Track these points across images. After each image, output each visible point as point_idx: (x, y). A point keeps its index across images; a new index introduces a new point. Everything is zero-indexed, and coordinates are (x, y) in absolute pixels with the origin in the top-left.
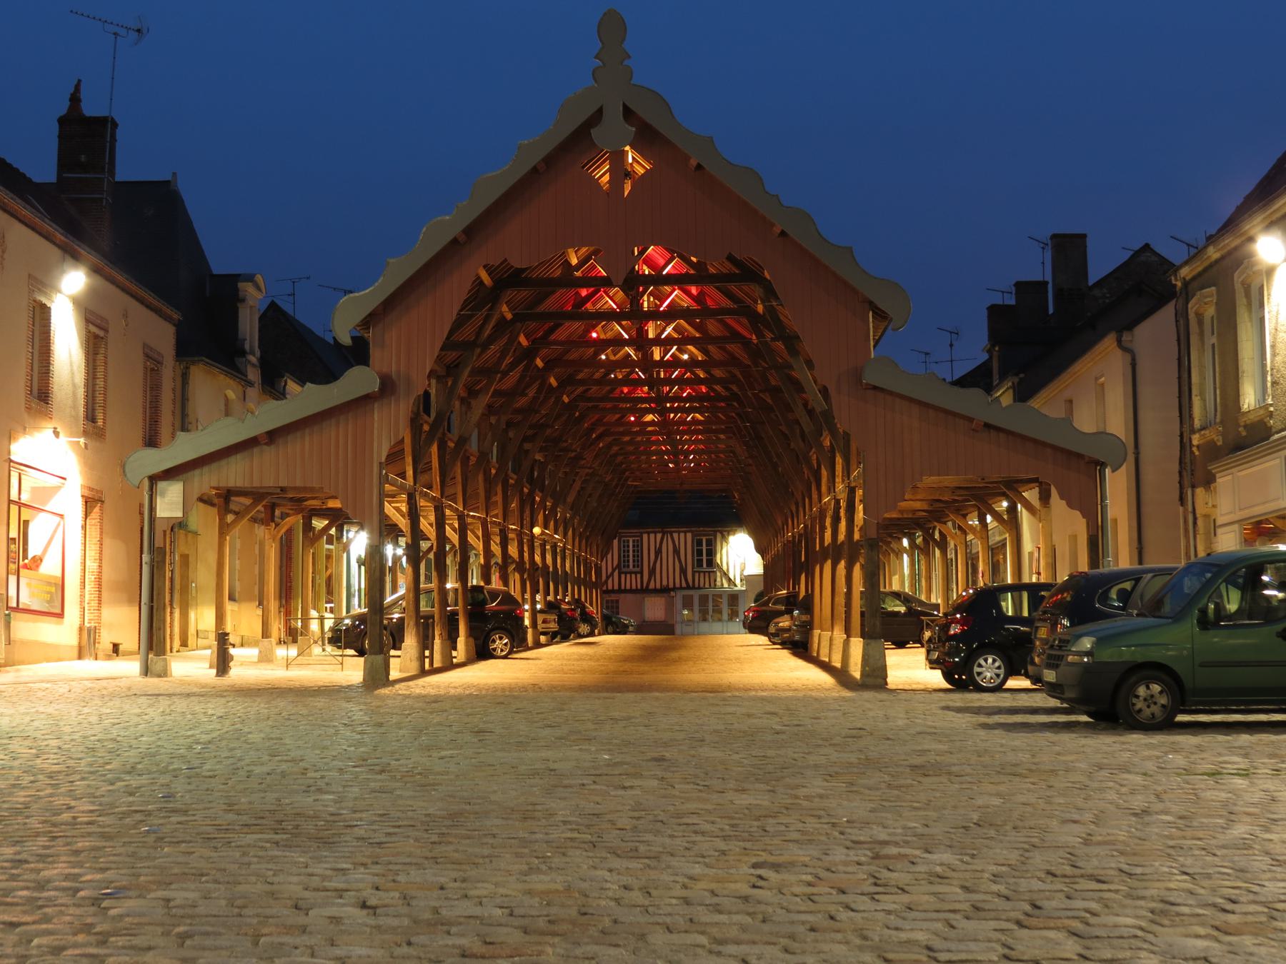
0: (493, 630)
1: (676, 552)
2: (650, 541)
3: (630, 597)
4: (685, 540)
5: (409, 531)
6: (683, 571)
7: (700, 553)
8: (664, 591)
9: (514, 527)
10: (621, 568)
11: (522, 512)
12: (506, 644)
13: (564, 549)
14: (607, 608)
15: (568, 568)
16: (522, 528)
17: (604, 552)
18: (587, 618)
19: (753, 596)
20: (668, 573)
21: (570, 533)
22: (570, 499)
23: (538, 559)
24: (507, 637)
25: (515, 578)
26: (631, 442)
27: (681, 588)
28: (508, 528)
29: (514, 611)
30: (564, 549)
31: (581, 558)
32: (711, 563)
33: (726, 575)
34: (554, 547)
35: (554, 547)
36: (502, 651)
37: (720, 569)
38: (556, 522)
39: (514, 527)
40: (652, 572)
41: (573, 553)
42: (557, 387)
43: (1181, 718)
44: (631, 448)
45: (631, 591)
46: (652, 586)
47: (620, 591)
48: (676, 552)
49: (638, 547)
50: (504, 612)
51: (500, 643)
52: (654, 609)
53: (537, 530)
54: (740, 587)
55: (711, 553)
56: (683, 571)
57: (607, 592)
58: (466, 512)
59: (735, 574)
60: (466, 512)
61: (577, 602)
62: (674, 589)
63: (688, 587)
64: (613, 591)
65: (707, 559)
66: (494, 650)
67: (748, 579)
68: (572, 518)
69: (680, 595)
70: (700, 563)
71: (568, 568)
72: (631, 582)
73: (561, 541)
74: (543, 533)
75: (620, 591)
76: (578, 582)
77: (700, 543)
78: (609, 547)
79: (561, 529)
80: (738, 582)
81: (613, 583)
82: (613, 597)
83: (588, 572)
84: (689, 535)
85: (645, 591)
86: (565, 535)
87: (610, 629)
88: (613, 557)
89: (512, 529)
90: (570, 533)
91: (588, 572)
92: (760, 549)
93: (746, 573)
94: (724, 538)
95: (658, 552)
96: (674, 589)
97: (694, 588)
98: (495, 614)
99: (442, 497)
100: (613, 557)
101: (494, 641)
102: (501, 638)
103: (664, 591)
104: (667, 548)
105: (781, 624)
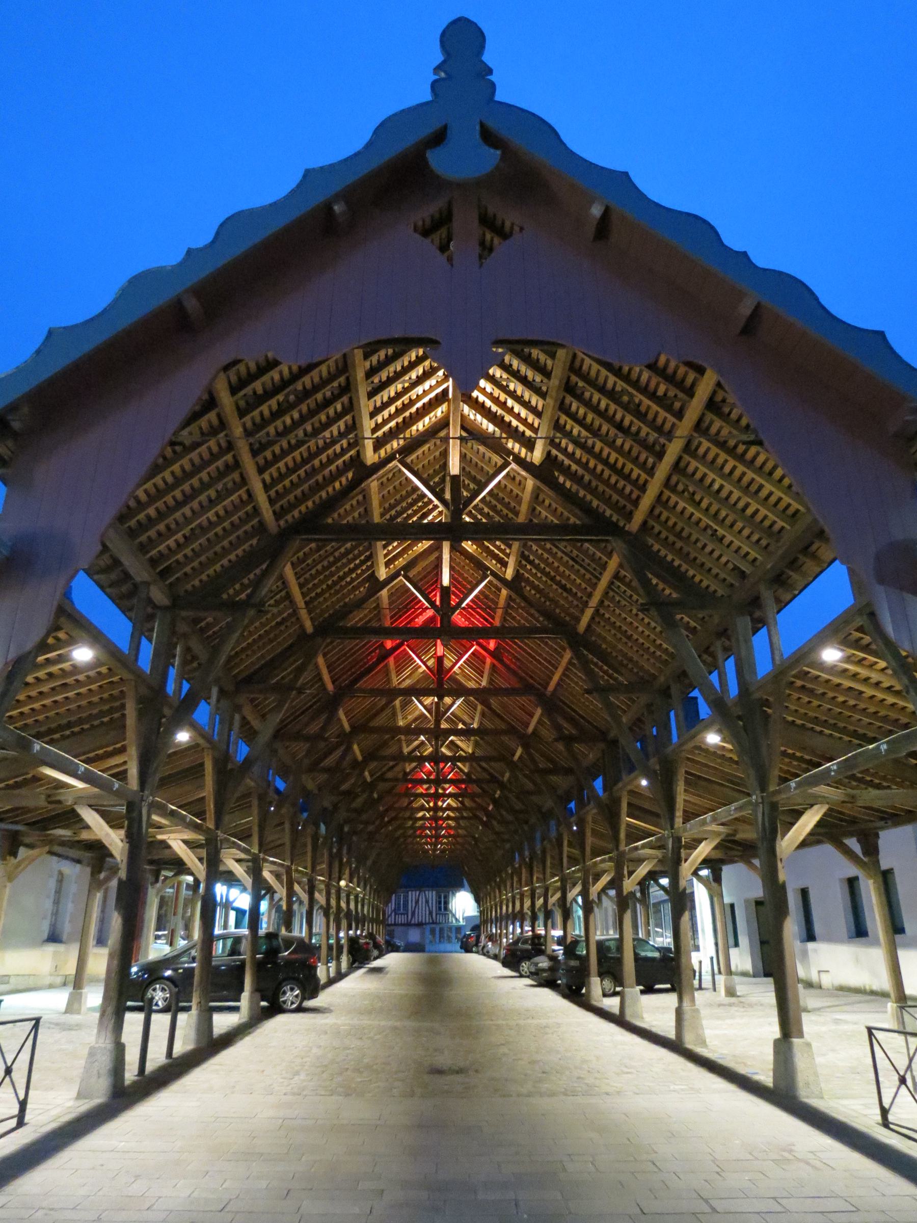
0: (284, 980)
1: (427, 902)
2: (412, 895)
3: (400, 929)
4: (432, 895)
5: (125, 861)
6: (431, 913)
7: (440, 903)
8: (420, 925)
9: (322, 878)
10: (396, 911)
11: (330, 866)
12: (297, 996)
13: (363, 899)
14: (388, 935)
15: (365, 912)
16: (330, 879)
17: (388, 901)
18: (377, 946)
19: (470, 928)
20: (422, 914)
21: (368, 888)
22: (369, 863)
23: (343, 905)
24: (299, 988)
25: (319, 921)
26: (412, 827)
27: (429, 923)
28: (316, 879)
29: (307, 959)
30: (363, 899)
31: (559, 919)
32: (446, 908)
33: (454, 916)
34: (357, 897)
35: (357, 897)
36: (292, 1003)
37: (451, 912)
38: (359, 878)
39: (322, 878)
40: (413, 913)
41: (369, 902)
42: (362, 761)
43: (657, 986)
44: (411, 832)
45: (402, 925)
46: (413, 922)
47: (395, 925)
48: (427, 902)
49: (406, 898)
50: (296, 961)
51: (290, 996)
52: (414, 936)
53: (343, 883)
54: (462, 923)
55: (446, 903)
56: (431, 913)
57: (389, 925)
58: (261, 855)
59: (459, 915)
60: (261, 855)
61: (371, 936)
62: (426, 924)
63: (433, 923)
64: (391, 925)
65: (443, 906)
66: (284, 1002)
67: (467, 919)
68: (370, 877)
69: (428, 927)
70: (440, 909)
71: (365, 912)
72: (401, 919)
73: (361, 892)
74: (347, 886)
75: (395, 925)
76: (372, 921)
77: (440, 897)
78: (389, 901)
79: (362, 884)
80: (461, 920)
81: (391, 920)
82: (392, 928)
83: (378, 915)
84: (434, 893)
85: (408, 925)
86: (365, 889)
87: (390, 948)
88: (392, 905)
89: (320, 880)
90: (368, 888)
91: (378, 915)
92: (478, 900)
93: (466, 915)
94: (454, 894)
95: (417, 902)
96: (426, 924)
97: (436, 923)
98: (289, 963)
99: (217, 828)
100: (392, 905)
101: (284, 993)
102: (292, 990)
103: (420, 925)
104: (422, 900)
105: (540, 965)
